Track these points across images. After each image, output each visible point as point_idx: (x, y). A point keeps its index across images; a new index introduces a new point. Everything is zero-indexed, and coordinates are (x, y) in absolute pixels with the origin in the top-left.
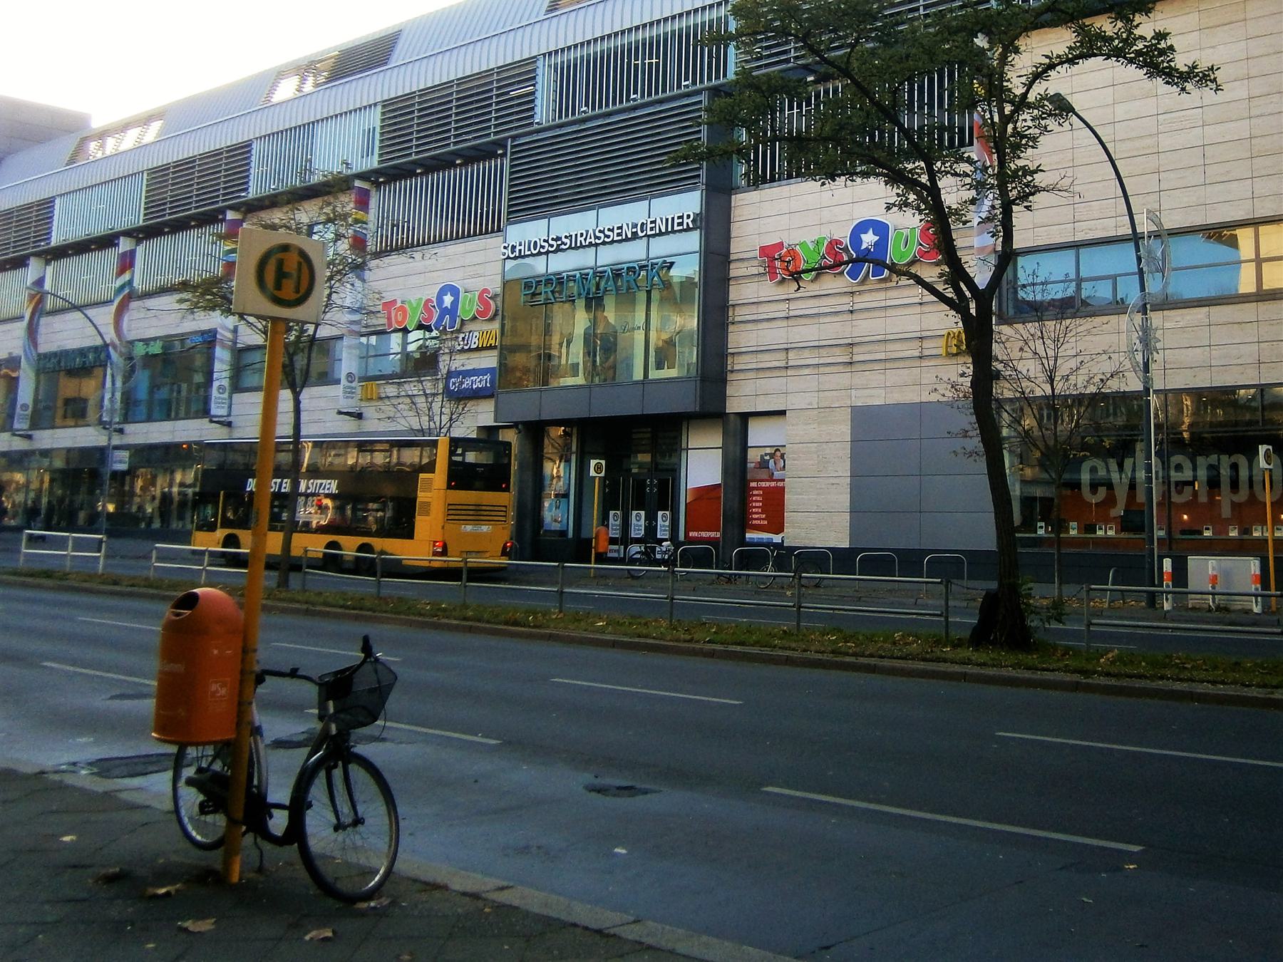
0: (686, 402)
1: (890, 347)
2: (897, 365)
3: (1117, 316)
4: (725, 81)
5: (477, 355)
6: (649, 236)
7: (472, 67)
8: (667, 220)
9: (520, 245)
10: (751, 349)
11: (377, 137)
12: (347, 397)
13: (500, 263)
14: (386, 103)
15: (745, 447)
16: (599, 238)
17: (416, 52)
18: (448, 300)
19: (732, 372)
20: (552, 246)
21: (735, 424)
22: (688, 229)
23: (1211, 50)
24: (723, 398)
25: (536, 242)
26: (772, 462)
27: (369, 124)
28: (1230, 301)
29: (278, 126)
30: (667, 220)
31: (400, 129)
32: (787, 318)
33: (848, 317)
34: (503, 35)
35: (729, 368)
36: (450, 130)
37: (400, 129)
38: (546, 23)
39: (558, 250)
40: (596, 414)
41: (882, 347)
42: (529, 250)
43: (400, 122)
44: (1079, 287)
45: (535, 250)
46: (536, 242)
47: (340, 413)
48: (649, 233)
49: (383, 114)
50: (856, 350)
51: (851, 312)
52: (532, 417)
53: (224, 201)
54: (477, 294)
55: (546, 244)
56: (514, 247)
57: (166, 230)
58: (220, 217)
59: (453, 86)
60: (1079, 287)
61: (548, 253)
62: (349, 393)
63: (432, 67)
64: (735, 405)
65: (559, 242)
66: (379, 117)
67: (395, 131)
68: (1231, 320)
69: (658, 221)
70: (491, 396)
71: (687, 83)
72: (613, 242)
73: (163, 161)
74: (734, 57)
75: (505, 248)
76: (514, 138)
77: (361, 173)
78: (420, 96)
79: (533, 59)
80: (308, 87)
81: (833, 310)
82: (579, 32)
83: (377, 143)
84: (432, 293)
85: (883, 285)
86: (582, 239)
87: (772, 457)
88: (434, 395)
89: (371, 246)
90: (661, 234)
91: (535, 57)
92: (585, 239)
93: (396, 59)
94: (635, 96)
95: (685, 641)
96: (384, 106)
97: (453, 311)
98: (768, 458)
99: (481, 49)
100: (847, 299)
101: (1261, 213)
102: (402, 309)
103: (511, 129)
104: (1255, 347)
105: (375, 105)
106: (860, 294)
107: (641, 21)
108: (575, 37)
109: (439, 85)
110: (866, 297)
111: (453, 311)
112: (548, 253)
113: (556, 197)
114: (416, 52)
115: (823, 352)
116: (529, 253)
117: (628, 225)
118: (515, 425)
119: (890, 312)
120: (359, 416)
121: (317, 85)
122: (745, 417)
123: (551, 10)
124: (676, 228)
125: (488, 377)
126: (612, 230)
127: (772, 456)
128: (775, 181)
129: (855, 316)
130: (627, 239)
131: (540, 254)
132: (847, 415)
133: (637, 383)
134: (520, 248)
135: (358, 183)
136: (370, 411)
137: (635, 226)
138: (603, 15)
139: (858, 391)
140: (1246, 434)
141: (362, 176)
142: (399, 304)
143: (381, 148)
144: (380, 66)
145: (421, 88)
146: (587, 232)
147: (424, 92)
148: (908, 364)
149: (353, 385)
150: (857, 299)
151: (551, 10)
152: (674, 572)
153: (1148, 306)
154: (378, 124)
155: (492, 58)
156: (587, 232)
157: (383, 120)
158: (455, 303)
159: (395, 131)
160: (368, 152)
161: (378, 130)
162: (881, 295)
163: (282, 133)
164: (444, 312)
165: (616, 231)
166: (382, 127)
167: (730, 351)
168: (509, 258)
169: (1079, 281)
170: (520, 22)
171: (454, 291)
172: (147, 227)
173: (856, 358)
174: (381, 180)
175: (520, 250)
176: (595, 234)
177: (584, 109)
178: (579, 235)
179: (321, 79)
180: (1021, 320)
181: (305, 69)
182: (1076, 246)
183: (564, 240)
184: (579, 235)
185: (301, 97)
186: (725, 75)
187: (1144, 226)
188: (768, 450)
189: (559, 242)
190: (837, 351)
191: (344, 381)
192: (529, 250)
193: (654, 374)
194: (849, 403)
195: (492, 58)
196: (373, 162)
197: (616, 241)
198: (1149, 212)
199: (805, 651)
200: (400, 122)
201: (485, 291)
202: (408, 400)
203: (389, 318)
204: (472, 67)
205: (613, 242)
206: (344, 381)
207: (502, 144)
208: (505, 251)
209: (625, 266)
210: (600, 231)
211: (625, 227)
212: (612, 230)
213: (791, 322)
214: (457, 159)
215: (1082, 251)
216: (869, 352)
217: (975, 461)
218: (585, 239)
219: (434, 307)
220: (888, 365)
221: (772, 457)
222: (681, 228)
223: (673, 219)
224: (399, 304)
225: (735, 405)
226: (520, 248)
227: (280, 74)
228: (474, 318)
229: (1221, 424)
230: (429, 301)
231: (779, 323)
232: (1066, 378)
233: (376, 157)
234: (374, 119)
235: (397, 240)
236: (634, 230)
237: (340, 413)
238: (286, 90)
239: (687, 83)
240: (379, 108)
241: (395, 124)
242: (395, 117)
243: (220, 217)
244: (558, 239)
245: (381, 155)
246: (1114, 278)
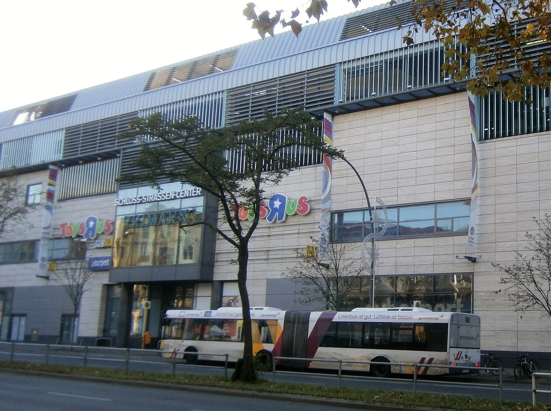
0: (195, 275)
1: (284, 252)
2: (287, 260)
3: (433, 238)
4: (220, 128)
5: (103, 250)
6: (182, 198)
7: (185, 95)
8: (189, 191)
9: (124, 200)
10: (225, 251)
11: (63, 144)
12: (41, 269)
13: (115, 207)
14: (68, 129)
15: (221, 296)
16: (159, 198)
17: (86, 105)
18: (277, 204)
19: (217, 262)
20: (138, 201)
21: (217, 285)
22: (198, 196)
23: (422, 126)
24: (212, 273)
25: (131, 199)
26: (233, 303)
27: (59, 139)
28: (462, 234)
29: (159, 102)
30: (189, 191)
31: (74, 142)
32: (298, 233)
33: (267, 238)
34: (261, 65)
35: (216, 260)
36: (275, 106)
37: (74, 142)
38: (143, 96)
39: (141, 203)
40: (153, 280)
41: (281, 252)
42: (128, 202)
43: (73, 139)
44: (436, 223)
45: (131, 202)
46: (131, 199)
47: (38, 276)
48: (181, 197)
49: (66, 134)
50: (270, 253)
51: (269, 236)
52: (126, 280)
53: (99, 150)
54: (105, 222)
55: (135, 200)
56: (121, 201)
57: (81, 162)
58: (118, 155)
59: (99, 123)
60: (436, 223)
61: (136, 204)
62: (42, 267)
63: (123, 105)
64: (217, 277)
65: (141, 199)
66: (64, 135)
67: (71, 142)
68: (423, 245)
69: (186, 191)
70: (108, 270)
71: (447, 79)
72: (165, 200)
73: (66, 125)
74: (224, 117)
75: (117, 201)
76: (124, 149)
77: (54, 162)
78: (102, 122)
79: (333, 66)
80: (32, 118)
81: (261, 235)
82: (206, 89)
83: (62, 148)
84: (84, 220)
85: (283, 224)
86: (152, 198)
87: (233, 301)
88: (76, 269)
89: (57, 196)
90: (186, 197)
91: (334, 64)
92: (153, 198)
93: (74, 108)
94: (410, 86)
95: (125, 379)
96: (66, 131)
97: (93, 229)
98: (231, 301)
99: (199, 85)
100: (267, 230)
101: (438, 198)
102: (70, 227)
103: (87, 152)
104: (432, 257)
105: (62, 129)
106: (273, 228)
107: (208, 92)
108: (176, 98)
109: (266, 81)
110: (276, 229)
111: (93, 229)
112: (136, 204)
113: (75, 188)
114: (86, 105)
115: (256, 254)
116: (128, 203)
117: (172, 192)
118: (119, 284)
119: (285, 237)
120: (47, 278)
121: (36, 118)
122: (222, 283)
123: (343, 38)
124: (193, 195)
125: (108, 260)
126: (165, 195)
127: (233, 300)
128: (311, 164)
129: (270, 238)
130: (171, 199)
131: (133, 204)
132: (264, 283)
133: (173, 266)
134: (124, 201)
135: (51, 167)
136: (52, 276)
137: (175, 193)
138: (237, 77)
139: (271, 272)
140: (379, 296)
141: (54, 163)
142: (68, 225)
143: (64, 150)
144: (65, 111)
145: (101, 119)
146: (154, 195)
147: (103, 120)
148: (291, 260)
149: (45, 263)
150: (272, 230)
151: (343, 38)
152: (129, 351)
153: (374, 239)
154: (63, 138)
155: (230, 83)
156: (154, 195)
157: (66, 137)
158: (282, 206)
159: (71, 142)
160: (59, 151)
161: (63, 142)
162: (282, 229)
163: (24, 139)
164: (90, 229)
165: (167, 195)
166: (65, 140)
167: (216, 252)
168: (119, 206)
169: (436, 220)
170: (251, 63)
171: (94, 220)
172: (64, 160)
173: (270, 257)
174: (63, 165)
175: (124, 202)
176: (157, 196)
177: (374, 93)
178: (150, 196)
179: (38, 115)
180: (360, 240)
181: (31, 109)
182: (398, 207)
183: (144, 198)
184: (150, 196)
185: (28, 123)
186: (220, 125)
187: (374, 204)
188: (232, 298)
189: (141, 199)
190: (262, 253)
191: (40, 261)
192: (128, 202)
193: (182, 261)
194: (266, 277)
195: (230, 83)
196: (60, 157)
197: (193, 197)
198: (377, 198)
199: (168, 382)
200: (73, 139)
201: (109, 220)
202: (63, 272)
203: (64, 231)
204: (185, 95)
205: (165, 200)
206: (40, 261)
207: (118, 152)
208: (117, 202)
209: (170, 212)
210: (160, 195)
211: (171, 193)
212: (165, 195)
213: (300, 235)
214: (98, 158)
215: (401, 209)
216: (275, 255)
217: (304, 305)
218: (153, 198)
219: (84, 227)
220: (283, 261)
221: (233, 301)
222: (195, 195)
223: (192, 190)
224: (68, 225)
225: (217, 277)
226: (124, 201)
227: (19, 111)
228: (296, 214)
229: (464, 288)
230: (83, 224)
231: (294, 236)
232: (345, 268)
233: (62, 155)
234: (61, 136)
235: (72, 193)
236: (175, 195)
237: (38, 276)
238: (21, 119)
239: (447, 79)
240: (64, 132)
241: (71, 139)
242: (72, 136)
243: (118, 155)
244: (141, 198)
245: (64, 153)
246: (452, 219)
